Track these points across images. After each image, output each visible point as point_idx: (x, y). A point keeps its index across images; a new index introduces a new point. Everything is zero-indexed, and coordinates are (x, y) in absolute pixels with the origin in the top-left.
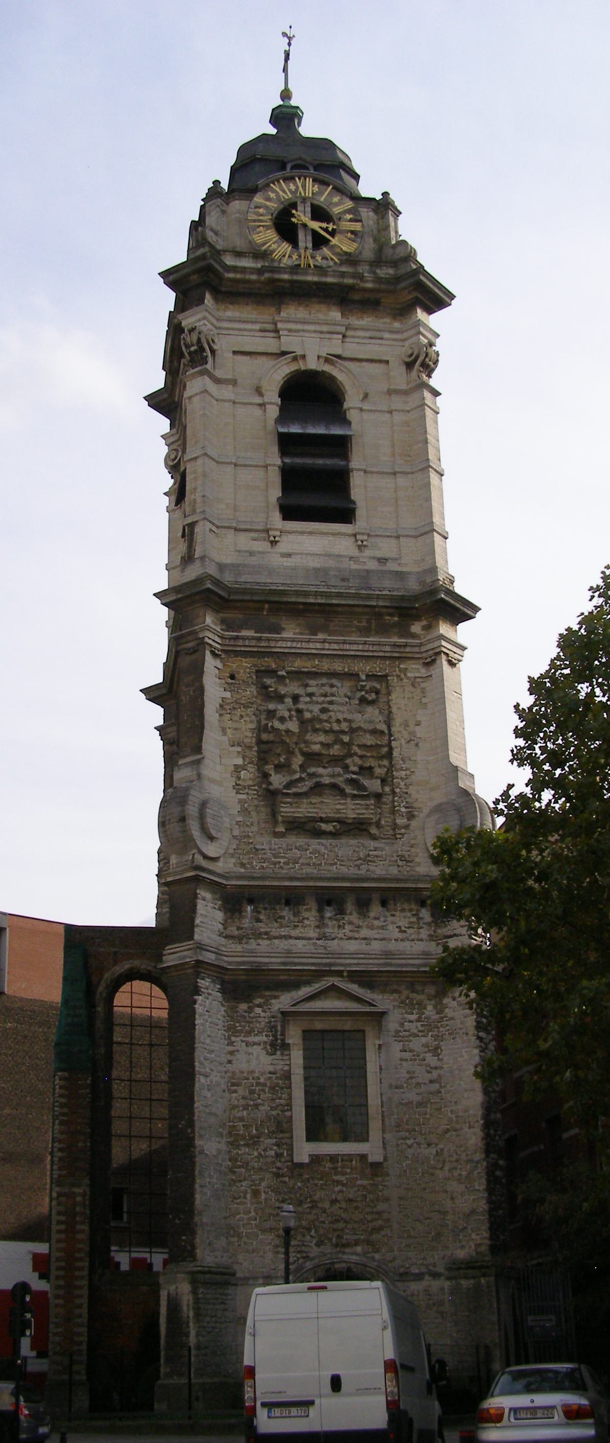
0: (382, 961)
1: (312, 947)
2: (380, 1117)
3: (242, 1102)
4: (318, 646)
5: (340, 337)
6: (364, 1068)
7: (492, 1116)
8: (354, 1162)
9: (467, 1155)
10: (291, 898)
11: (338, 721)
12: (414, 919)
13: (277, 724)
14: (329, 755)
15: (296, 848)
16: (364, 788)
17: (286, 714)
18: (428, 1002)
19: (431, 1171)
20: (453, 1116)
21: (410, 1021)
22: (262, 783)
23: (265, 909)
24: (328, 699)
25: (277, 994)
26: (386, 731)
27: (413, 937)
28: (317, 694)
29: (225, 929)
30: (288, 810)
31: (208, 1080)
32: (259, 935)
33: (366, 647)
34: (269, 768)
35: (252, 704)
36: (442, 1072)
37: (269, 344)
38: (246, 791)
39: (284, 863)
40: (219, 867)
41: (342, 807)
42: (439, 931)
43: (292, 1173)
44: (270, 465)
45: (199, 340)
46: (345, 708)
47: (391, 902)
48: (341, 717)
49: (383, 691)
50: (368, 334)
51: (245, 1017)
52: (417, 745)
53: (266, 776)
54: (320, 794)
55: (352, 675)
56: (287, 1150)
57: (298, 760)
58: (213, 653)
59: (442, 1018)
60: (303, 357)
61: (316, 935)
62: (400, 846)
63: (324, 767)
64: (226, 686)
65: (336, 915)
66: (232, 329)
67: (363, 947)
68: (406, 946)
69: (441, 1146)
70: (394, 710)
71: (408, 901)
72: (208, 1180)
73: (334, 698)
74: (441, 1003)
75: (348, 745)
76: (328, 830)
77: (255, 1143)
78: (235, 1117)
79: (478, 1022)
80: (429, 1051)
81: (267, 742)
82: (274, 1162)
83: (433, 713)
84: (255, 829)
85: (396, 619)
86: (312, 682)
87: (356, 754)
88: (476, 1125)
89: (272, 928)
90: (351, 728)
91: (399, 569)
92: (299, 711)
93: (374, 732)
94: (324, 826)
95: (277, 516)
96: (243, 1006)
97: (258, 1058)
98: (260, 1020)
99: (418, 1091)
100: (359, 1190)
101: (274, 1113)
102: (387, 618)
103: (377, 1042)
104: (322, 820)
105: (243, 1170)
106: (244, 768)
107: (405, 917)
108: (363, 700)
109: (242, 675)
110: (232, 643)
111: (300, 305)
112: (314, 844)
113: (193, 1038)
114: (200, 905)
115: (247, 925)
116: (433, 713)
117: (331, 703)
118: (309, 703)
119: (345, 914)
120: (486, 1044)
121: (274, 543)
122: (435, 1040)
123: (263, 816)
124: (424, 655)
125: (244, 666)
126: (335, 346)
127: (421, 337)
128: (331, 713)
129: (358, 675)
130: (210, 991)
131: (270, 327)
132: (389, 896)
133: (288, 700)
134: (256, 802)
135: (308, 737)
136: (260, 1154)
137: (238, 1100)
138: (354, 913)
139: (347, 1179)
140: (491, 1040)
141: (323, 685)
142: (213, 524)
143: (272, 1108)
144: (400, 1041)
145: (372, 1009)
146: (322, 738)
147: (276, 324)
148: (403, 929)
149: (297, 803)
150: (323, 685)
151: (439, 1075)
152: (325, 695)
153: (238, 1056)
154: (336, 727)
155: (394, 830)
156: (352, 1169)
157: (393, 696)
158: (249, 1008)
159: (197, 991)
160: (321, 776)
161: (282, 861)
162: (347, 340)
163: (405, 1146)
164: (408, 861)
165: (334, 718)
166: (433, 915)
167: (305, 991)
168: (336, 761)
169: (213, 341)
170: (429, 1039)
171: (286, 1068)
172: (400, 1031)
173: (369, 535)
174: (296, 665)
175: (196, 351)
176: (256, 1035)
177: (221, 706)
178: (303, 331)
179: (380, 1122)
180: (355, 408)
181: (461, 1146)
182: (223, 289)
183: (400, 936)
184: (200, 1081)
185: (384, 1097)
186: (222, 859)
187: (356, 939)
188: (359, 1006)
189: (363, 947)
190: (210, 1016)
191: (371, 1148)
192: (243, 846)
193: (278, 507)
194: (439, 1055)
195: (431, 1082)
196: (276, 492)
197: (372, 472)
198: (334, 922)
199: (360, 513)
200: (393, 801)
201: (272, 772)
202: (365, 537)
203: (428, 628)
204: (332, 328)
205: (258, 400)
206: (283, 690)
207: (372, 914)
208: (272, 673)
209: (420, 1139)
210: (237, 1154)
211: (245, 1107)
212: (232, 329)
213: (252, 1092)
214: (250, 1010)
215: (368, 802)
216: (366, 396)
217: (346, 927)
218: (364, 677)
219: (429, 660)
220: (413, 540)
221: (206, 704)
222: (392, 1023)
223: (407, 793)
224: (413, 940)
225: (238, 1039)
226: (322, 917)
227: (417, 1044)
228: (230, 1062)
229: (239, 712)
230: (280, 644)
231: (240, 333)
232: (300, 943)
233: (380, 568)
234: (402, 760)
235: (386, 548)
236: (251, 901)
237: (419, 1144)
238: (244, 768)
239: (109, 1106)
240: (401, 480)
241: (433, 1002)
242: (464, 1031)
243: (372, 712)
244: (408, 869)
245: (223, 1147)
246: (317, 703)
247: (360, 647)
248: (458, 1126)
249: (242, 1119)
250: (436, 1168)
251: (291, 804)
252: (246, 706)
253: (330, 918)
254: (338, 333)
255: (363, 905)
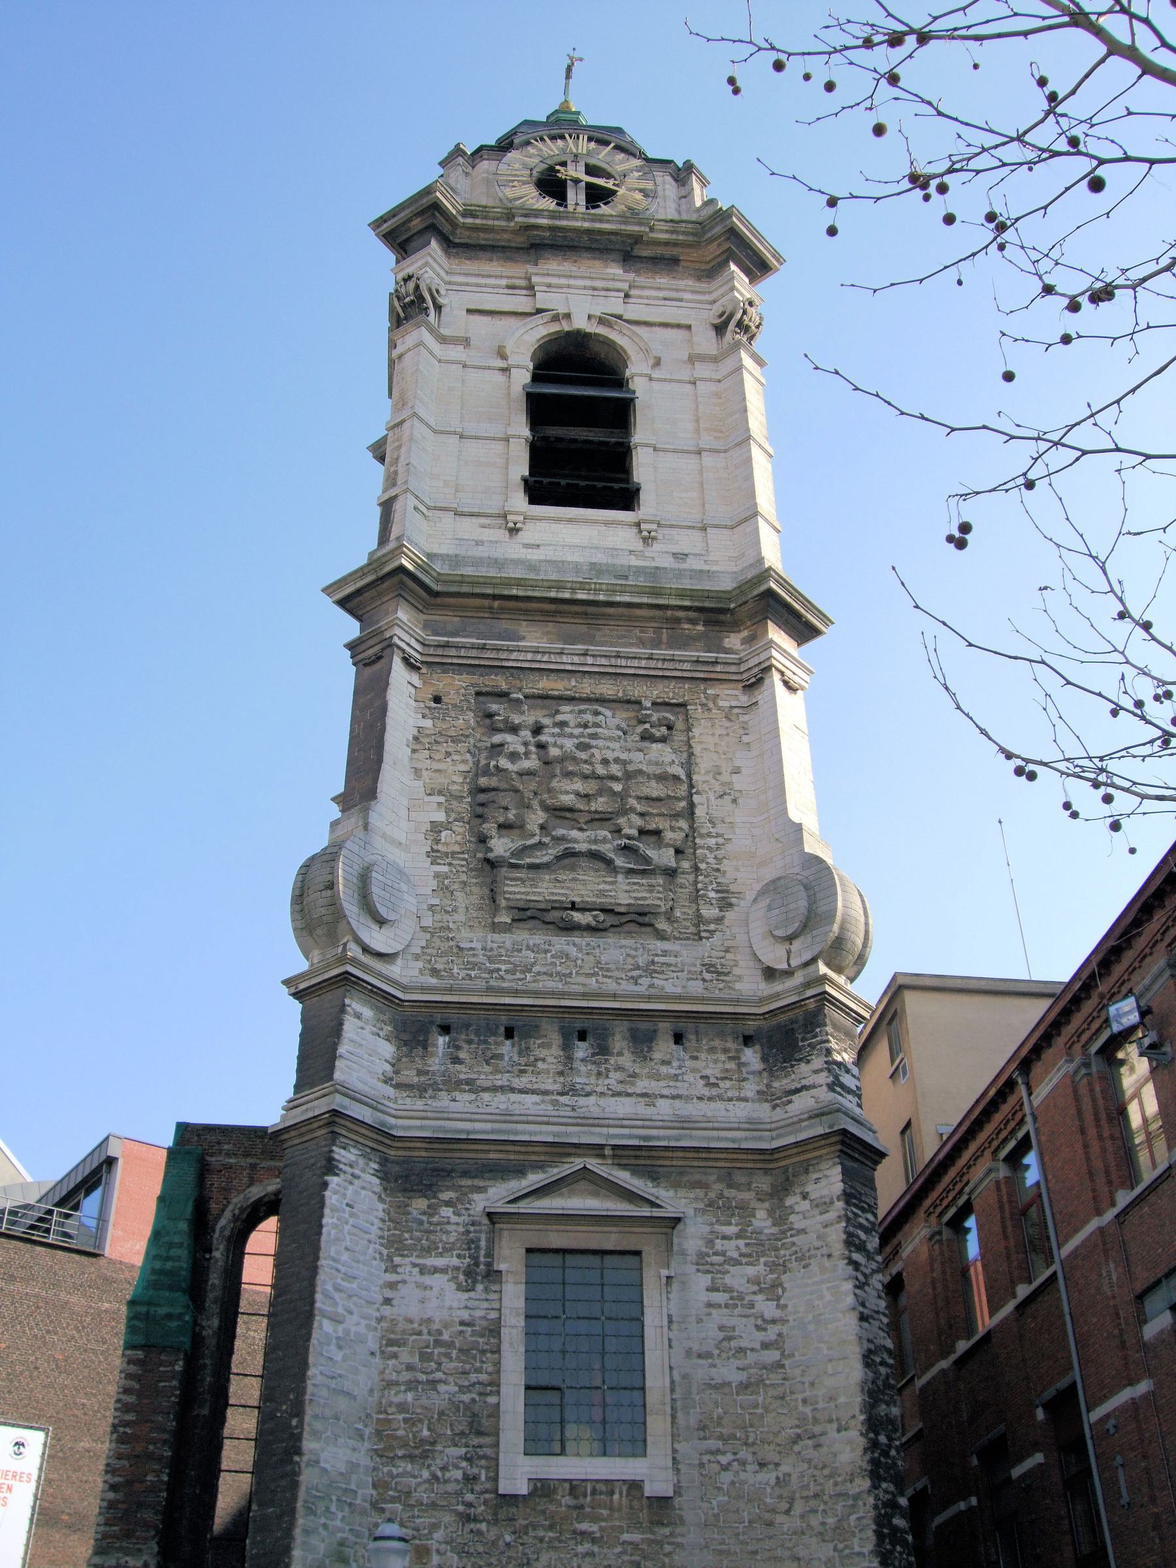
0: (675, 1132)
1: (550, 1107)
2: (668, 1409)
3: (406, 1376)
4: (576, 659)
5: (622, 295)
6: (638, 1320)
7: (882, 1409)
8: (616, 1497)
9: (836, 1484)
10: (516, 1025)
11: (605, 762)
12: (732, 1065)
13: (504, 763)
14: (589, 812)
15: (528, 948)
16: (647, 860)
17: (522, 749)
18: (758, 1205)
19: (767, 1516)
20: (808, 1410)
21: (724, 1238)
22: (476, 851)
23: (470, 1042)
24: (589, 731)
25: (481, 1183)
26: (683, 777)
27: (730, 1094)
28: (572, 724)
29: (397, 1072)
30: (516, 889)
31: (340, 1328)
32: (455, 1085)
33: (652, 664)
34: (490, 828)
35: (467, 736)
36: (785, 1330)
37: (521, 303)
38: (449, 860)
39: (507, 971)
40: (395, 970)
41: (608, 887)
42: (776, 1084)
43: (495, 1514)
44: (514, 436)
45: (417, 287)
46: (616, 745)
47: (692, 1037)
48: (610, 756)
49: (680, 725)
50: (661, 294)
51: (421, 1223)
52: (734, 801)
53: (483, 840)
54: (573, 868)
55: (629, 702)
56: (487, 1468)
57: (536, 818)
58: (406, 661)
59: (784, 1232)
60: (568, 316)
61: (557, 1087)
62: (707, 949)
63: (581, 829)
64: (427, 711)
65: (593, 1055)
66: (467, 284)
67: (642, 1109)
68: (716, 1110)
69: (784, 1468)
70: (697, 750)
71: (722, 1035)
72: (323, 1520)
73: (599, 730)
74: (781, 1206)
75: (622, 796)
76: (584, 922)
77: (425, 1455)
78: (390, 1404)
79: (850, 1235)
80: (761, 1291)
81: (483, 790)
82: (459, 1493)
83: (761, 755)
84: (460, 917)
85: (700, 628)
86: (566, 708)
87: (632, 810)
88: (852, 1423)
89: (479, 1073)
90: (626, 772)
91: (706, 568)
92: (541, 746)
93: (662, 778)
94: (577, 916)
95: (519, 501)
96: (420, 1204)
97: (441, 1295)
98: (450, 1228)
99: (740, 1363)
100: (624, 1552)
101: (466, 1398)
102: (686, 626)
103: (665, 1272)
104: (573, 907)
105: (399, 1507)
106: (447, 826)
107: (716, 1062)
108: (646, 737)
109: (451, 698)
110: (440, 652)
111: (565, 260)
112: (560, 943)
113: (316, 1248)
114: (350, 1026)
115: (436, 1068)
116: (761, 755)
117: (594, 736)
118: (559, 735)
119: (612, 1054)
120: (865, 1275)
121: (514, 531)
122: (771, 1272)
123: (474, 899)
124: (745, 676)
125: (456, 686)
126: (615, 305)
127: (736, 294)
128: (594, 750)
129: (639, 703)
130: (357, 1172)
131: (523, 283)
132: (685, 1027)
133: (526, 734)
134: (464, 877)
135: (554, 784)
136: (435, 1477)
137: (398, 1373)
138: (626, 1052)
139: (601, 1529)
140: (874, 1271)
141: (580, 712)
142: (422, 502)
143: (462, 1389)
144: (708, 1272)
145: (656, 1212)
146: (578, 785)
147: (530, 280)
148: (712, 1080)
149: (533, 880)
150: (580, 712)
151: (780, 1335)
152: (586, 726)
153: (404, 1290)
154: (601, 770)
155: (697, 925)
156: (611, 1509)
157: (696, 731)
158: (429, 1207)
159: (331, 1166)
160: (575, 841)
161: (503, 967)
162: (631, 300)
163: (716, 1467)
164: (719, 974)
165: (598, 757)
166: (764, 1059)
167: (534, 1179)
168: (600, 819)
169: (437, 291)
170: (761, 1268)
171: (493, 1315)
172: (708, 1255)
173: (659, 525)
174: (540, 685)
175: (412, 302)
176: (441, 1255)
177: (416, 739)
178: (569, 287)
179: (669, 1419)
180: (641, 375)
181: (824, 1467)
182: (457, 241)
183: (706, 1092)
184: (323, 1328)
185: (675, 1373)
186: (399, 961)
187: (628, 1095)
188: (632, 1207)
189: (642, 1109)
190: (352, 1215)
191: (652, 1471)
192: (437, 943)
193: (522, 487)
194: (778, 1299)
195: (765, 1346)
196: (522, 468)
197: (665, 450)
198: (593, 1067)
199: (646, 497)
200: (696, 882)
201: (494, 833)
202: (654, 527)
203: (751, 640)
204: (610, 285)
205: (501, 364)
206: (517, 719)
207: (657, 1056)
208: (502, 695)
209: (744, 1454)
210: (390, 1474)
211: (412, 1385)
212: (467, 284)
213: (425, 1357)
214: (432, 1210)
215: (653, 882)
216: (657, 363)
217: (611, 1074)
218: (649, 705)
219: (753, 680)
220: (729, 532)
221: (388, 728)
222: (692, 1236)
223: (718, 870)
224: (730, 1100)
225: (407, 1260)
226: (570, 1058)
227: (738, 1277)
228: (388, 1301)
229: (443, 748)
230: (514, 656)
231: (479, 289)
232: (530, 1099)
233: (676, 565)
234: (711, 821)
235: (688, 542)
236: (445, 1029)
237: (743, 1463)
238: (447, 826)
239: (219, 1419)
240: (707, 459)
241: (767, 1205)
242: (825, 1251)
243: (663, 755)
244: (721, 986)
245: (365, 1460)
246: (571, 736)
247: (643, 663)
248: (817, 1429)
249: (402, 1407)
250: (774, 1511)
251: (523, 881)
252: (455, 740)
253: (582, 1060)
254: (618, 290)
255: (642, 1041)
